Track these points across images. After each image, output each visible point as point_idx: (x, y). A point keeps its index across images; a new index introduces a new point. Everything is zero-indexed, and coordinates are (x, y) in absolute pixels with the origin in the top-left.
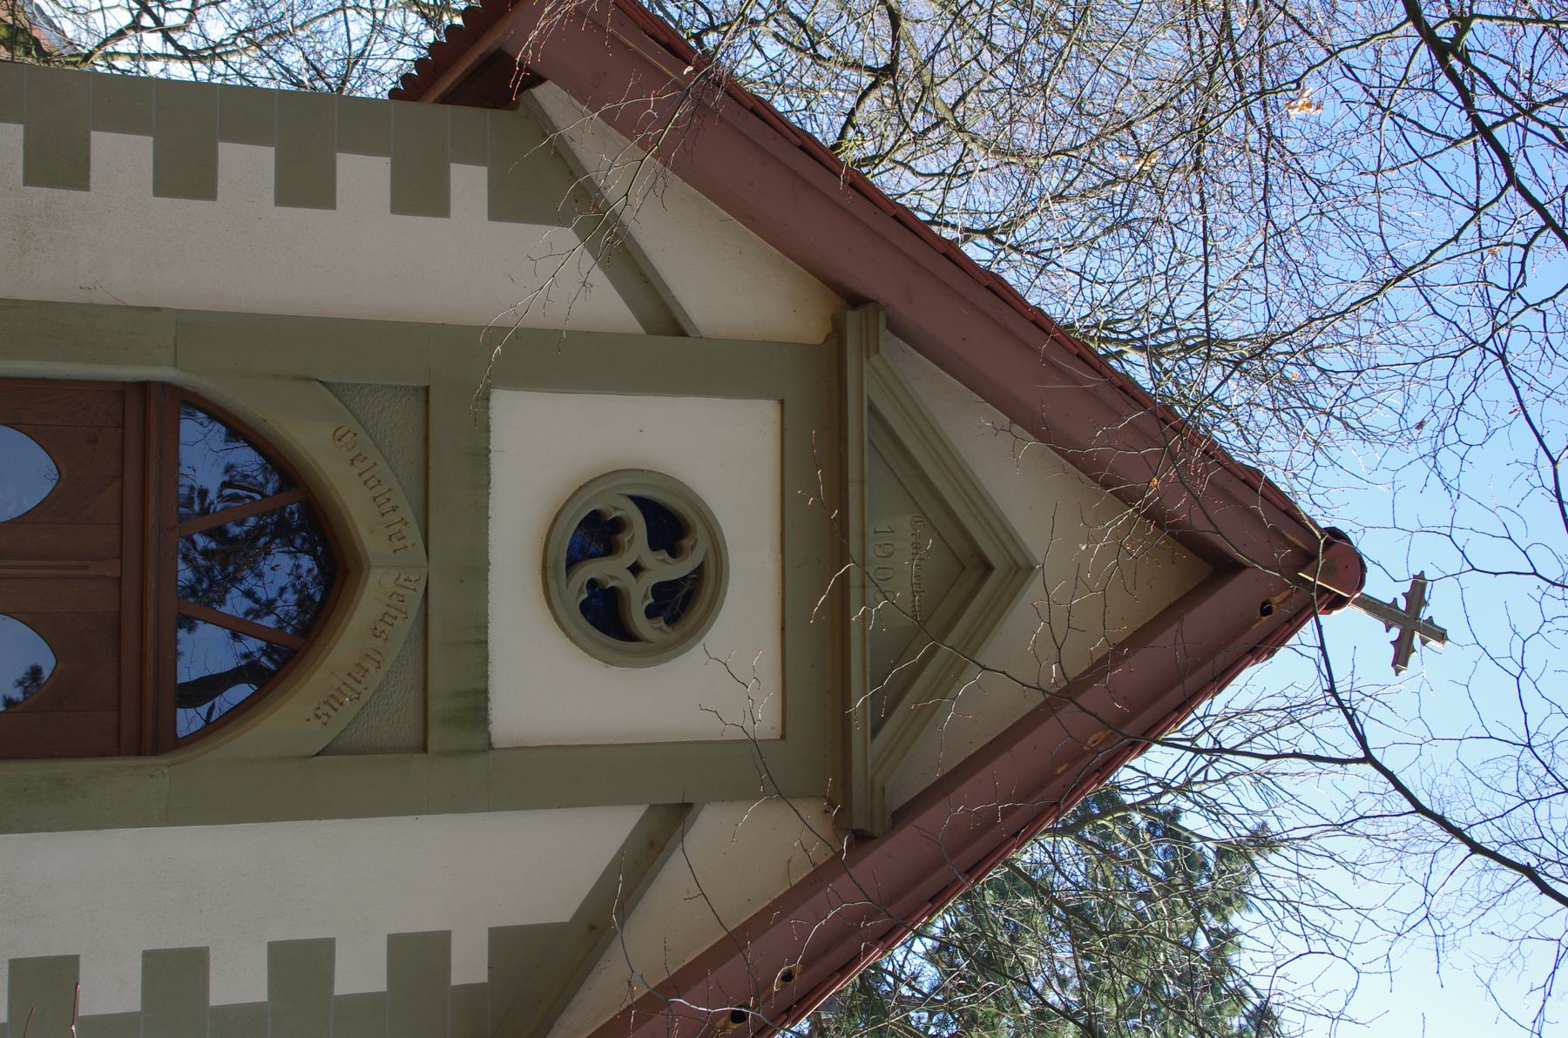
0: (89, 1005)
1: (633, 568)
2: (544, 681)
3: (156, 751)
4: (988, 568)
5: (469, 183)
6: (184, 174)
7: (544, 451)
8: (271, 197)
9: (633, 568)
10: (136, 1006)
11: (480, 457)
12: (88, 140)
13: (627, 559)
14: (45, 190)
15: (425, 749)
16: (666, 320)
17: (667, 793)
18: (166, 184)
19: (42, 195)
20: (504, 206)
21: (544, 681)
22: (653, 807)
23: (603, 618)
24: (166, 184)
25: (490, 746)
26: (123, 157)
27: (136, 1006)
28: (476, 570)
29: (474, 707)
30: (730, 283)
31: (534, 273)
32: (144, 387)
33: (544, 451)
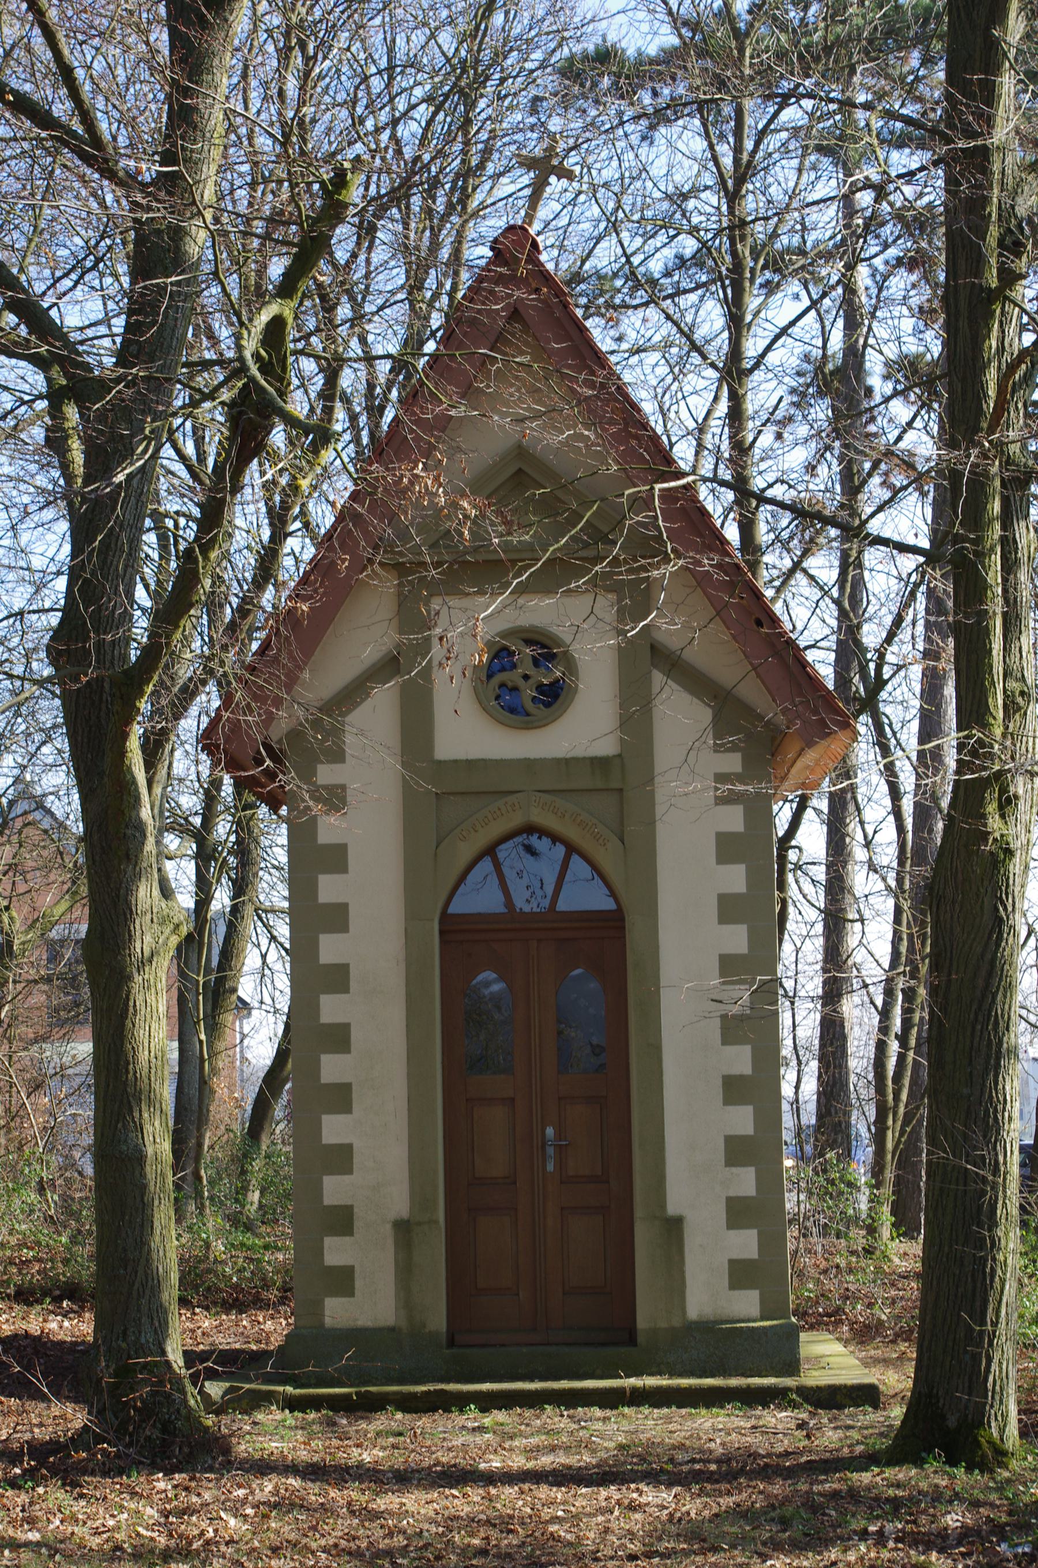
0: (747, 1070)
1: (527, 679)
2: (588, 727)
3: (623, 920)
4: (520, 469)
5: (326, 774)
6: (337, 918)
7: (466, 732)
8: (344, 876)
9: (527, 679)
10: (745, 927)
11: (471, 765)
12: (325, 965)
13: (521, 683)
14: (351, 983)
15: (621, 790)
16: (390, 665)
17: (649, 659)
18: (345, 1107)
19: (353, 985)
20: (338, 756)
21: (588, 727)
22: (655, 667)
23: (554, 696)
24: (345, 1107)
25: (620, 756)
26: (332, 1009)
27: (745, 927)
28: (529, 765)
29: (600, 764)
30: (366, 633)
31: (373, 727)
32: (443, 942)
33: (466, 732)
